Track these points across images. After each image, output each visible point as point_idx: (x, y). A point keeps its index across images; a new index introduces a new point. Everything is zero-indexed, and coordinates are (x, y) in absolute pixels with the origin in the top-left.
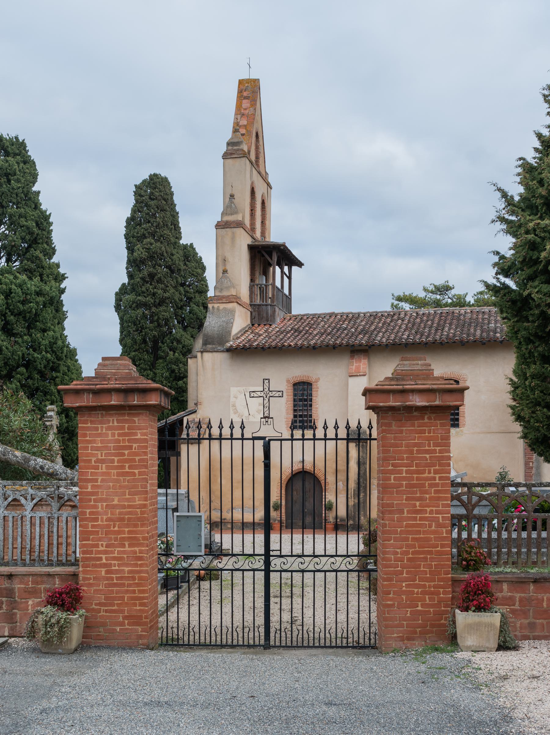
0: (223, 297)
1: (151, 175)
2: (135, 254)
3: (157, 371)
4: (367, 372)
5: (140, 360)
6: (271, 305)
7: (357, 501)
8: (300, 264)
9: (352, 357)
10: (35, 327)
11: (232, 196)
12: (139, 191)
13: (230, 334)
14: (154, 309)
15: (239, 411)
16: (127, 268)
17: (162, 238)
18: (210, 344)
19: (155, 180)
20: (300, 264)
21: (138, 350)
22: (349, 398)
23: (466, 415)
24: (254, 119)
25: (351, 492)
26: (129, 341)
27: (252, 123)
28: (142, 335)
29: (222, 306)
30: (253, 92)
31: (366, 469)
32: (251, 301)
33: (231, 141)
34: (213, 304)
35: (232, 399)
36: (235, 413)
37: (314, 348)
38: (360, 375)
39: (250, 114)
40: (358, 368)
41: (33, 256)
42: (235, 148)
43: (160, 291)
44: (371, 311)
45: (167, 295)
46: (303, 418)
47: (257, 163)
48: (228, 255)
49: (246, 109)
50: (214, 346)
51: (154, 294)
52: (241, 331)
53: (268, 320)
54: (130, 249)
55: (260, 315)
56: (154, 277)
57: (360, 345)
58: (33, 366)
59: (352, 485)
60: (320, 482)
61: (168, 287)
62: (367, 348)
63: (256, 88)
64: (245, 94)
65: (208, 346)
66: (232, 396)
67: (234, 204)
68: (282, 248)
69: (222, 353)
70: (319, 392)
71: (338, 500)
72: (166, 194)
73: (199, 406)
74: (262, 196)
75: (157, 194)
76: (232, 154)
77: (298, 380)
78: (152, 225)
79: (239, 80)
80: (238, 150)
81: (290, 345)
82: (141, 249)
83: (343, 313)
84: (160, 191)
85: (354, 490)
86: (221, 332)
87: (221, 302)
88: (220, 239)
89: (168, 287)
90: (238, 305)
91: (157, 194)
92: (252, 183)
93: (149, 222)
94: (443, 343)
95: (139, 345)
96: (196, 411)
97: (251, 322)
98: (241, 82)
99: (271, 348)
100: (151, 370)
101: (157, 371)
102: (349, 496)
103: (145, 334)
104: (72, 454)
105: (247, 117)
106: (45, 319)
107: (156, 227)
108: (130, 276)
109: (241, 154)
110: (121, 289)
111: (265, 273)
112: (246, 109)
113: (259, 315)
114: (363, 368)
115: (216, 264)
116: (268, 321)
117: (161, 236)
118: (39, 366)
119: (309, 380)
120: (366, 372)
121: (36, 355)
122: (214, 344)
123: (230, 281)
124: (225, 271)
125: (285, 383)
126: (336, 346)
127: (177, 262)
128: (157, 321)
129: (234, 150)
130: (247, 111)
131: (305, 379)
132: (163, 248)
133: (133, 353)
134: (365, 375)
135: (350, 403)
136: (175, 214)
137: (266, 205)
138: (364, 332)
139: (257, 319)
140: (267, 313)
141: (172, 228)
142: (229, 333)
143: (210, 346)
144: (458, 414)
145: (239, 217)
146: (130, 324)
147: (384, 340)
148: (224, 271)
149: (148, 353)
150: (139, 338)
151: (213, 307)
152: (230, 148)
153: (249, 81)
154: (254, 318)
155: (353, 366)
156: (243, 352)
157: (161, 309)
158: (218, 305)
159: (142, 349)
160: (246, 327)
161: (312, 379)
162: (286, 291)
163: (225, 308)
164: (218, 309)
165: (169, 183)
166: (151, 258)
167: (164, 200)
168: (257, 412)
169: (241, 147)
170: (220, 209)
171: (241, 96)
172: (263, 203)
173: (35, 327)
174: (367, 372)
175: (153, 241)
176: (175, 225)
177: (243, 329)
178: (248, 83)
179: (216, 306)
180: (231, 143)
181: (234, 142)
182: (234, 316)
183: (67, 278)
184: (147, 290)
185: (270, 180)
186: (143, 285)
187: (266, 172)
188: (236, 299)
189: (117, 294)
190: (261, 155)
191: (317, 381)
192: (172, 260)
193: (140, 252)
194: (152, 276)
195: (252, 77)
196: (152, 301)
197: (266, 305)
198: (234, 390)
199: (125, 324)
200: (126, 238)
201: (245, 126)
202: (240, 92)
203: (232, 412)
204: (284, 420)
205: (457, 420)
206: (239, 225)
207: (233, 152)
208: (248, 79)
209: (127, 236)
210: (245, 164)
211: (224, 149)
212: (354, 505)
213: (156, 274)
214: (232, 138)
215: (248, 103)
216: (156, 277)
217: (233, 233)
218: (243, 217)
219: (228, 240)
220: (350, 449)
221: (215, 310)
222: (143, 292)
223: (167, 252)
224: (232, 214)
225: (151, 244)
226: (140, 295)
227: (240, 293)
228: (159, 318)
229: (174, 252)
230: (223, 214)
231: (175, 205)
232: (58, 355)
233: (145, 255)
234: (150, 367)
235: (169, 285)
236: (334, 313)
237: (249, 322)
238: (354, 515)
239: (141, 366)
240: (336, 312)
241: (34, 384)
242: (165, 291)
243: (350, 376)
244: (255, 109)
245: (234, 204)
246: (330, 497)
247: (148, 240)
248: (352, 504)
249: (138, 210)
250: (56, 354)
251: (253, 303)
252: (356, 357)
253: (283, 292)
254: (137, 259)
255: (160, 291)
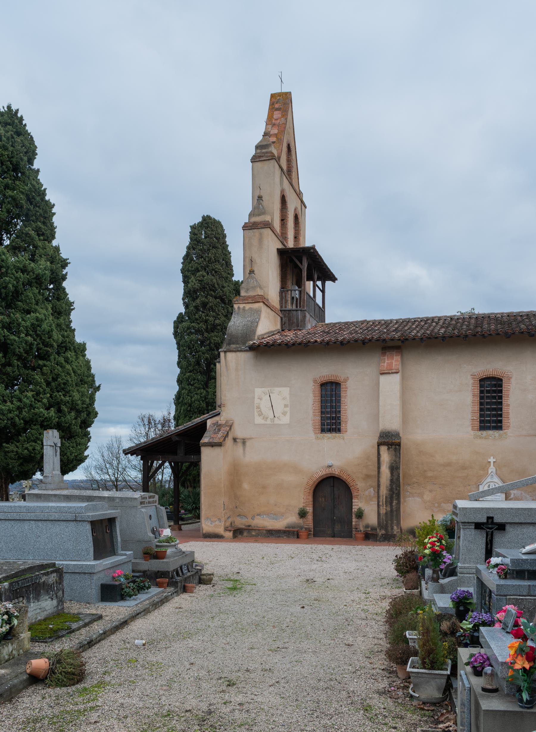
0: (249, 297)
1: (204, 216)
2: (189, 285)
3: (209, 390)
4: (400, 369)
5: (194, 380)
6: (301, 310)
7: (389, 509)
8: (333, 279)
9: (384, 354)
10: (16, 307)
11: (260, 198)
12: (195, 230)
13: (255, 333)
14: (206, 334)
15: (264, 413)
16: (183, 299)
17: (213, 272)
18: (233, 344)
19: (208, 221)
20: (333, 279)
21: (193, 370)
22: (381, 398)
23: (511, 416)
24: (285, 128)
25: (383, 499)
26: (184, 363)
27: (283, 131)
28: (196, 358)
29: (248, 306)
30: (285, 104)
31: (399, 474)
32: (281, 307)
33: (260, 144)
34: (238, 305)
35: (257, 401)
36: (260, 415)
37: (342, 343)
38: (392, 373)
39: (281, 123)
40: (390, 365)
41: (23, 233)
42: (264, 151)
43: (211, 319)
44: (403, 318)
45: (217, 322)
46: (331, 420)
47: (290, 172)
48: (255, 256)
49: (277, 119)
50: (238, 346)
51: (206, 321)
52: (268, 333)
53: (299, 325)
54: (186, 280)
55: (289, 319)
56: (206, 305)
57: (392, 340)
58: (11, 350)
59: (384, 491)
60: (349, 488)
61: (219, 315)
62: (400, 343)
63: (287, 101)
64: (277, 106)
65: (232, 346)
66: (256, 397)
67: (262, 206)
68: (312, 251)
69: (245, 353)
70: (349, 393)
71: (368, 507)
72: (218, 233)
73: (222, 408)
74: (295, 210)
75: (209, 232)
76: (260, 157)
77: (326, 379)
78: (205, 260)
79: (271, 94)
80: (267, 153)
81: (316, 341)
82: (194, 281)
83: (375, 320)
84: (212, 231)
85: (386, 497)
86: (245, 331)
87: (246, 302)
88: (247, 241)
89: (219, 315)
90: (265, 306)
91: (209, 232)
92: (282, 191)
93: (202, 257)
94: (486, 335)
95: (193, 367)
96: (219, 414)
97: (282, 327)
98: (273, 96)
99: (296, 344)
100: (204, 389)
101: (209, 390)
102: (381, 503)
103: (199, 356)
104: (68, 454)
105: (278, 126)
106: (29, 299)
107: (208, 261)
108: (187, 306)
109: (269, 156)
110: (178, 318)
111: (299, 283)
112: (277, 119)
113: (289, 320)
114: (396, 365)
115: (244, 266)
116: (298, 326)
117: (213, 270)
118: (17, 350)
119: (338, 380)
120: (398, 370)
121: (12, 337)
122: (238, 344)
123: (256, 281)
124: (252, 272)
125: (312, 384)
126: (366, 341)
127: (227, 294)
128: (209, 345)
129: (263, 153)
130: (278, 121)
131: (333, 379)
132: (214, 281)
133: (188, 374)
134: (397, 373)
135: (381, 403)
136: (227, 253)
137: (300, 220)
138: (396, 330)
139: (287, 324)
140: (297, 319)
141: (223, 264)
142: (254, 332)
143: (234, 346)
144: (501, 415)
145: (268, 218)
146: (185, 348)
147: (419, 335)
148: (250, 271)
149: (201, 373)
150: (192, 360)
151: (239, 308)
152: (259, 151)
153: (280, 94)
154: (285, 324)
155: (384, 363)
156: (266, 350)
157: (212, 334)
158: (244, 305)
159: (196, 370)
160: (274, 331)
161: (341, 377)
162: (319, 301)
163: (251, 308)
164: (244, 309)
165: (222, 226)
166: (203, 288)
167: (216, 238)
168: (282, 414)
169: (270, 149)
170: (249, 208)
171: (272, 108)
172: (296, 217)
173: (16, 307)
174: (400, 369)
175: (205, 273)
176: (226, 263)
177: (271, 332)
178: (280, 96)
179: (242, 306)
180: (260, 146)
181: (263, 145)
182: (260, 315)
183: (70, 263)
184: (200, 317)
185: (304, 199)
186: (196, 313)
187: (300, 190)
188: (263, 300)
189: (175, 322)
190: (294, 169)
191: (346, 380)
192: (223, 292)
193: (194, 283)
194: (204, 305)
195: (284, 90)
196: (205, 327)
197: (297, 310)
198: (258, 391)
199: (181, 349)
200: (182, 273)
201: (276, 135)
202: (272, 104)
203: (256, 414)
204: (311, 422)
205: (501, 421)
206: (268, 225)
207: (262, 155)
208: (280, 93)
209: (183, 271)
210: (274, 167)
211: (253, 152)
212: (386, 513)
213: (208, 303)
214: (261, 142)
215: (279, 114)
216: (208, 306)
217: (261, 234)
218: (272, 220)
219: (255, 242)
220: (381, 453)
221: (241, 311)
222: (197, 319)
223: (218, 284)
224: (259, 215)
225: (203, 276)
226: (194, 322)
227: (268, 295)
228: (210, 342)
229: (225, 285)
230: (250, 215)
231: (228, 246)
232: (44, 340)
233: (197, 285)
234: (203, 386)
235: (220, 313)
236: (366, 320)
237: (279, 327)
238: (386, 524)
239: (195, 385)
240: (368, 319)
241: (13, 372)
242: (216, 318)
243: (382, 374)
244: (286, 119)
245: (262, 206)
246: (357, 504)
247: (201, 273)
248: (384, 512)
249: (193, 247)
250: (41, 339)
251: (284, 309)
252: (387, 353)
253: (315, 301)
254: (190, 290)
255: (211, 319)
